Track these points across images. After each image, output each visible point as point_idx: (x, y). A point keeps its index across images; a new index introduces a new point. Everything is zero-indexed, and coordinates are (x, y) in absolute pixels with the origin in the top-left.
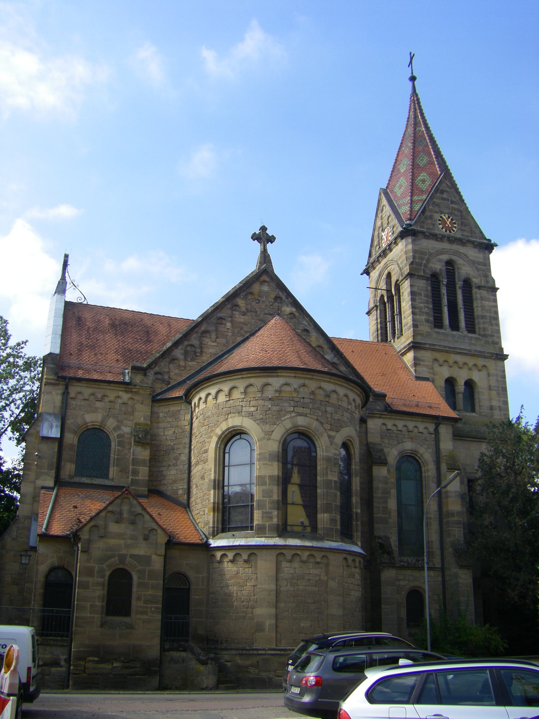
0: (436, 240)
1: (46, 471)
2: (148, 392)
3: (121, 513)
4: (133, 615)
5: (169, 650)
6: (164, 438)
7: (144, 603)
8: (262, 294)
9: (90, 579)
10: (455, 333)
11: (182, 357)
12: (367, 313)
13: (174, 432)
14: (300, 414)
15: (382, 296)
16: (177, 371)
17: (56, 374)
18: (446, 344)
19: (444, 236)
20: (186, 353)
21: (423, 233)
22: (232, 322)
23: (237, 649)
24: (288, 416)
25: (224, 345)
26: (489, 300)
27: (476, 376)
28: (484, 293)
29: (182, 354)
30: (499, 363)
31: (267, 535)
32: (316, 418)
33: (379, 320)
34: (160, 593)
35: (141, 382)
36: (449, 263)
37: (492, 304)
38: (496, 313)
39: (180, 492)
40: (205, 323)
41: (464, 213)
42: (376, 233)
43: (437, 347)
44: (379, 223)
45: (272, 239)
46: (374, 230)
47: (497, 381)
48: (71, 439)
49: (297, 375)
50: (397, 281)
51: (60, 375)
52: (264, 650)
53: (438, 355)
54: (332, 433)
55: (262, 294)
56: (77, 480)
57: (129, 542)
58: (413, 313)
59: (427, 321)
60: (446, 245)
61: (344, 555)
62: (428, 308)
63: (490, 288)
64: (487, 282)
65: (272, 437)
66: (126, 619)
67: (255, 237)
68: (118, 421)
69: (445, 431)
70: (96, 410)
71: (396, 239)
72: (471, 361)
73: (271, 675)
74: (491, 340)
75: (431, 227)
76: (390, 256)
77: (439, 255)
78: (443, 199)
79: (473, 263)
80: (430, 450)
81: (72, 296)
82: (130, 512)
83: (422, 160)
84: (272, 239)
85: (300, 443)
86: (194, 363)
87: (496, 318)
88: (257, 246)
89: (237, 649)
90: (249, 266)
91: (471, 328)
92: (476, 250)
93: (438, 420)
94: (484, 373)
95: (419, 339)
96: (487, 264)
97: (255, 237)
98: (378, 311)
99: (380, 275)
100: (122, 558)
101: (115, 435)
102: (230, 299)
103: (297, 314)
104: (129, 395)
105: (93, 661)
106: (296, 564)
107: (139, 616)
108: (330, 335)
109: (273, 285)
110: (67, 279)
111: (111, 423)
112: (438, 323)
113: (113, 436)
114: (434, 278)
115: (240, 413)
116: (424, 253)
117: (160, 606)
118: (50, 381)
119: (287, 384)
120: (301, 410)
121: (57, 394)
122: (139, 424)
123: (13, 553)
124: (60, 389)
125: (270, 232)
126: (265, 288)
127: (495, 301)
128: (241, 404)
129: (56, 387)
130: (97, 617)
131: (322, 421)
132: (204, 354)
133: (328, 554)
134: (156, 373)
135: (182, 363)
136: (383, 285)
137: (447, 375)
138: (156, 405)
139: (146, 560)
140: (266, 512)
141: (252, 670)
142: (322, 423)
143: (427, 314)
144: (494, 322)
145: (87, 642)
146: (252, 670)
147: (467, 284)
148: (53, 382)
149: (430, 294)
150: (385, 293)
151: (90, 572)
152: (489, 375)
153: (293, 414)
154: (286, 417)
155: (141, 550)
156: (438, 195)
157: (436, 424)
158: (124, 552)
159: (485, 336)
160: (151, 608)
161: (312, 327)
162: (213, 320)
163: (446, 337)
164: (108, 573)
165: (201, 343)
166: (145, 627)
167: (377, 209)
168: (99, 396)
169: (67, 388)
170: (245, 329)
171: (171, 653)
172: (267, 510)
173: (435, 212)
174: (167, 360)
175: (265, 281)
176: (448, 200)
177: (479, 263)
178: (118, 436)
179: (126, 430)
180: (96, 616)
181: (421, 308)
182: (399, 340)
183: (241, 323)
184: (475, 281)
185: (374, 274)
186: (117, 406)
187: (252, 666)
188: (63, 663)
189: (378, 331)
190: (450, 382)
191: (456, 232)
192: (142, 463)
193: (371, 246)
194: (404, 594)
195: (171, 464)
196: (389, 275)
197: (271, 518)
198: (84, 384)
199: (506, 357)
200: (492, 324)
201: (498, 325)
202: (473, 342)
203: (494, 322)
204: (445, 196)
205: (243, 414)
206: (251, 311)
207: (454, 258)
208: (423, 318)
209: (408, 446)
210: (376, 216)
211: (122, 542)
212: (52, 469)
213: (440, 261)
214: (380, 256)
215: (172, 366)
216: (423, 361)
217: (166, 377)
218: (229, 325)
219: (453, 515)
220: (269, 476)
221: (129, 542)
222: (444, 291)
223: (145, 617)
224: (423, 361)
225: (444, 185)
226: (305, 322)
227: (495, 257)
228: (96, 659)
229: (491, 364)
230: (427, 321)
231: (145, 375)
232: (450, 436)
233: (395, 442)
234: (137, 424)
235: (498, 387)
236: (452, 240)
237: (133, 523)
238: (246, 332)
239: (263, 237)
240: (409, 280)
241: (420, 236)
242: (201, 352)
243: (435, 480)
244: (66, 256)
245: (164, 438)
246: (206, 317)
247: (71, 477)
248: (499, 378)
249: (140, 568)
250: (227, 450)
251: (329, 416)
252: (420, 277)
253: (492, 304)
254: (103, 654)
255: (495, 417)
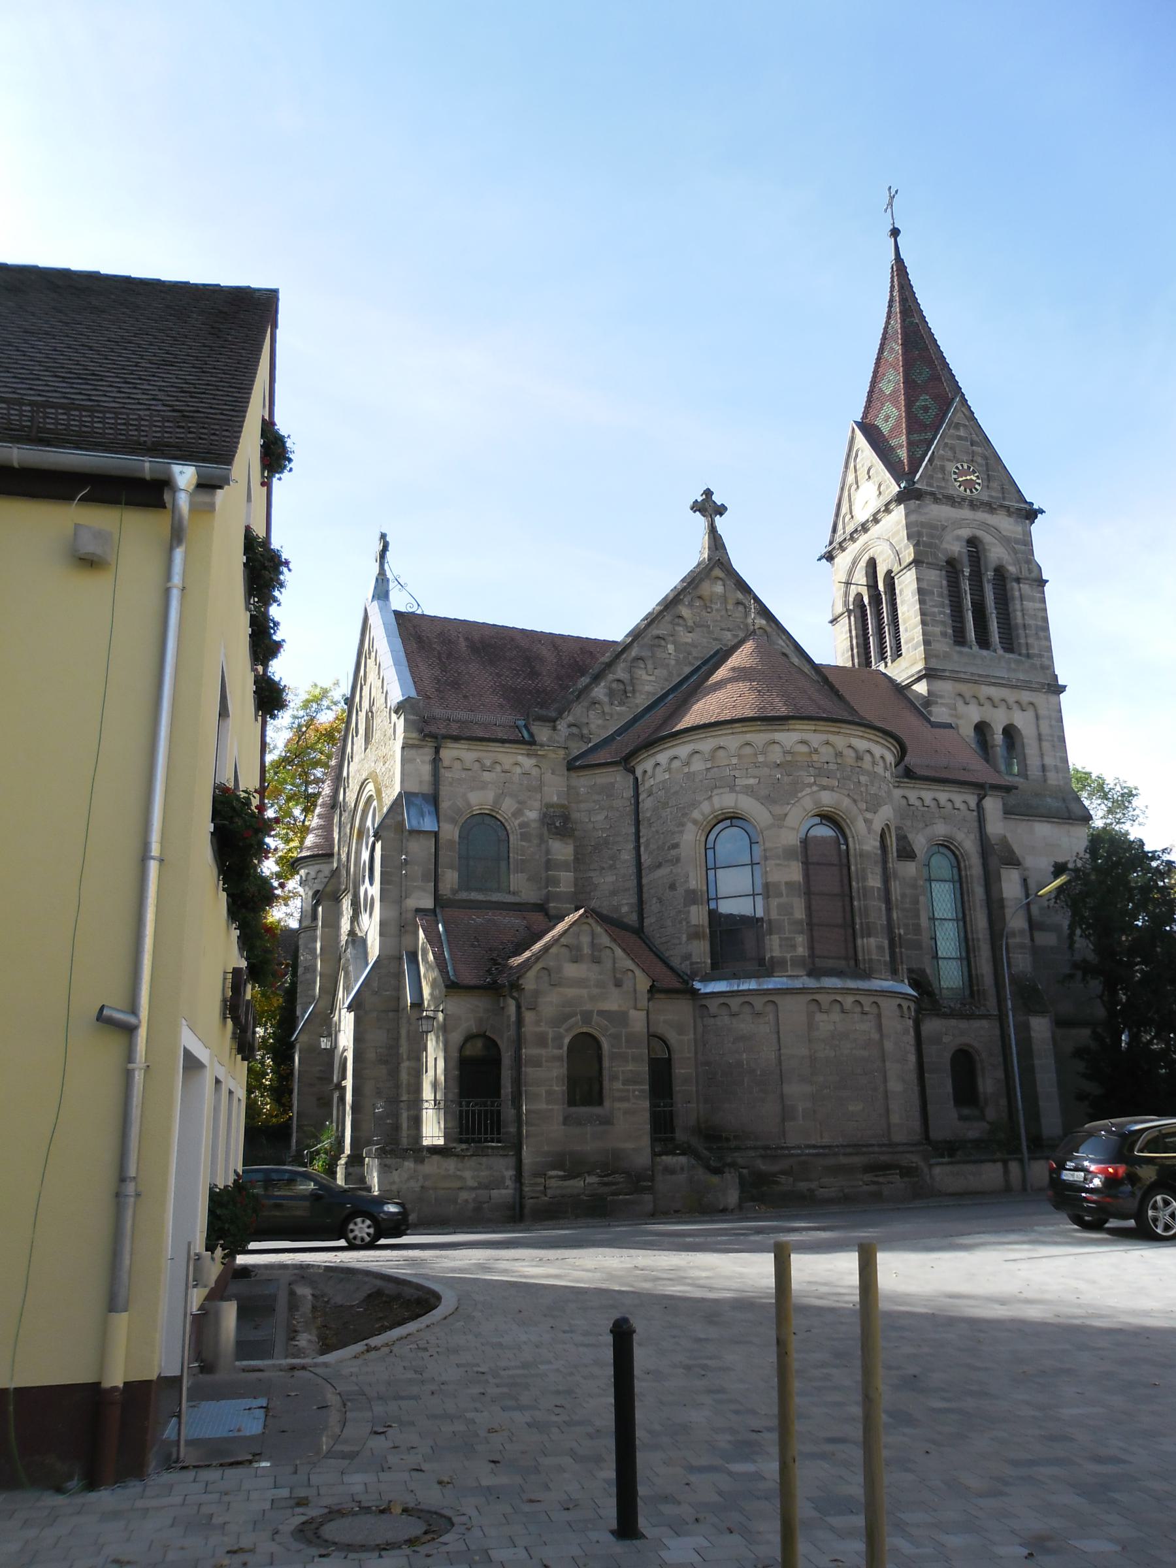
0: (953, 506)
1: (420, 883)
2: (562, 752)
3: (578, 948)
4: (607, 1104)
5: (660, 1155)
6: (591, 826)
7: (624, 1084)
8: (715, 598)
9: (543, 1052)
10: (985, 653)
11: (606, 699)
12: (831, 622)
13: (607, 817)
14: (824, 788)
15: (859, 596)
16: (600, 722)
17: (421, 731)
18: (971, 669)
19: (964, 499)
20: (611, 693)
21: (932, 494)
22: (674, 643)
23: (755, 1148)
24: (808, 790)
25: (666, 680)
26: (1032, 599)
27: (1023, 721)
28: (1025, 588)
29: (605, 695)
30: (1052, 698)
31: (789, 973)
32: (846, 792)
33: (854, 633)
34: (645, 1068)
35: (549, 740)
36: (973, 542)
37: (1038, 605)
38: (1045, 619)
39: (625, 909)
40: (635, 644)
41: (992, 461)
42: (846, 494)
43: (963, 676)
44: (851, 478)
45: (721, 510)
46: (842, 489)
47: (1051, 726)
48: (450, 832)
49: (818, 728)
50: (889, 572)
51: (427, 731)
52: (799, 1147)
53: (964, 688)
54: (869, 816)
55: (715, 598)
56: (464, 895)
57: (595, 991)
58: (923, 623)
59: (944, 634)
60: (966, 513)
61: (899, 1001)
62: (944, 613)
63: (1035, 580)
64: (1030, 571)
65: (786, 823)
66: (596, 1110)
67: (697, 507)
68: (519, 802)
69: (992, 805)
70: (483, 786)
71: (887, 505)
72: (1011, 696)
73: (813, 1185)
74: (1038, 663)
75: (943, 484)
76: (875, 530)
77: (957, 526)
78: (960, 438)
79: (1006, 541)
80: (972, 836)
81: (399, 601)
82: (593, 945)
83: (920, 374)
84: (721, 510)
85: (825, 831)
86: (623, 708)
87: (1046, 628)
88: (700, 521)
89: (755, 1148)
90: (691, 553)
91: (1009, 644)
92: (1011, 520)
93: (981, 789)
94: (1030, 714)
95: (934, 664)
96: (1027, 542)
97: (697, 507)
98: (852, 618)
99: (855, 563)
100: (587, 1017)
101: (517, 822)
102: (670, 604)
103: (768, 629)
104: (533, 761)
105: (558, 1177)
106: (836, 1016)
107: (617, 1105)
108: (817, 660)
109: (730, 583)
110: (389, 575)
111: (507, 807)
112: (959, 638)
113: (513, 825)
114: (951, 567)
115: (732, 788)
116: (933, 527)
117: (647, 1087)
118: (411, 742)
119: (803, 742)
120: (825, 781)
121: (423, 762)
122: (552, 806)
123: (375, 1014)
124: (427, 753)
125: (718, 499)
126: (719, 588)
127: (1043, 601)
128: (732, 773)
129: (421, 751)
130: (558, 1109)
131: (855, 797)
132: (638, 694)
133: (880, 1000)
134: (570, 726)
135: (607, 709)
136: (860, 577)
137: (976, 719)
138: (574, 775)
139: (619, 1018)
140: (787, 939)
141: (783, 1179)
142: (855, 801)
143: (943, 623)
144: (1042, 634)
145: (546, 1148)
146: (783, 1179)
147: (1000, 572)
148: (417, 742)
149: (946, 592)
150: (864, 591)
151: (542, 1041)
152: (1037, 717)
153: (815, 788)
154: (804, 793)
155: (613, 1003)
156: (952, 431)
157: (979, 795)
158: (588, 1007)
159: (1028, 656)
160: (634, 1091)
161: (792, 648)
162: (647, 639)
163: (974, 659)
164: (567, 1041)
165: (632, 678)
166: (627, 1124)
167: (848, 456)
168: (488, 763)
169: (437, 750)
170: (695, 654)
171: (664, 1157)
172: (787, 935)
173: (949, 460)
174: (585, 704)
175: (718, 578)
176: (966, 439)
177: (1017, 542)
178: (521, 826)
179: (532, 815)
180: (556, 1107)
181: (933, 614)
182: (895, 664)
183: (686, 643)
184: (1012, 569)
185: (843, 560)
186: (516, 778)
187: (783, 1172)
188: (508, 1182)
189: (852, 650)
190: (982, 729)
191: (980, 492)
192: (564, 866)
193: (837, 515)
194: (947, 1056)
195: (605, 865)
196: (872, 564)
197: (794, 947)
198: (463, 745)
199: (1062, 689)
200: (1038, 638)
201: (1048, 639)
202: (1013, 666)
203: (1042, 634)
204: (962, 433)
205: (738, 788)
206: (703, 626)
207: (979, 533)
208: (937, 630)
209: (941, 829)
210: (846, 467)
211: (584, 992)
212: (429, 881)
213: (958, 538)
214: (856, 531)
215: (592, 713)
216: (941, 697)
217: (585, 731)
218: (671, 648)
219: (1013, 934)
220: (786, 883)
221: (595, 991)
222: (966, 586)
223: (625, 1105)
224: (941, 697)
225: (960, 415)
226: (781, 642)
227: (1038, 529)
228: (561, 1173)
229: (1040, 699)
230: (944, 634)
231: (554, 729)
232: (1000, 813)
233: (921, 825)
234: (549, 806)
235: (1052, 736)
236: (974, 505)
237: (596, 961)
238: (696, 658)
239: (708, 507)
240: (914, 570)
241: (928, 500)
242: (634, 691)
243: (982, 882)
244: (383, 536)
245: (591, 826)
246: (636, 635)
247: (455, 892)
248: (1053, 723)
249: (612, 1030)
250: (710, 845)
251: (863, 789)
252: (931, 565)
253: (1038, 605)
254: (572, 1165)
255: (1050, 782)
